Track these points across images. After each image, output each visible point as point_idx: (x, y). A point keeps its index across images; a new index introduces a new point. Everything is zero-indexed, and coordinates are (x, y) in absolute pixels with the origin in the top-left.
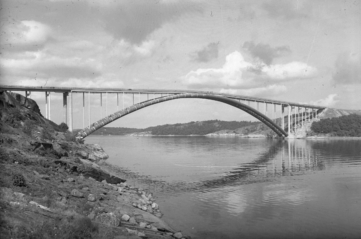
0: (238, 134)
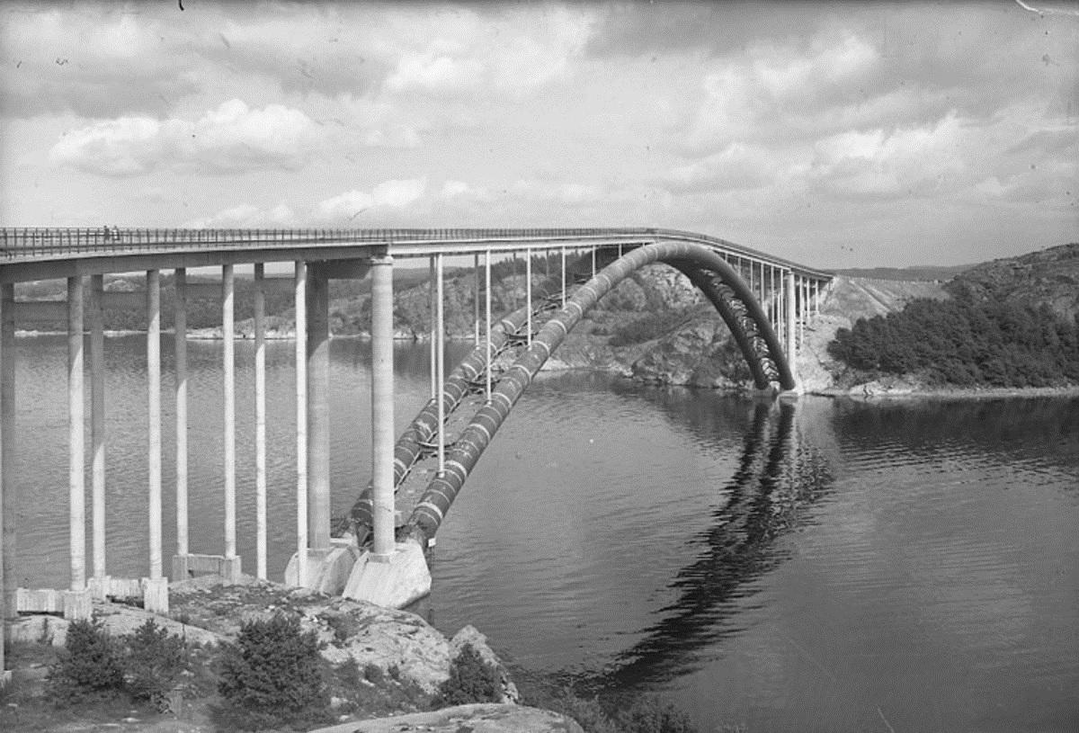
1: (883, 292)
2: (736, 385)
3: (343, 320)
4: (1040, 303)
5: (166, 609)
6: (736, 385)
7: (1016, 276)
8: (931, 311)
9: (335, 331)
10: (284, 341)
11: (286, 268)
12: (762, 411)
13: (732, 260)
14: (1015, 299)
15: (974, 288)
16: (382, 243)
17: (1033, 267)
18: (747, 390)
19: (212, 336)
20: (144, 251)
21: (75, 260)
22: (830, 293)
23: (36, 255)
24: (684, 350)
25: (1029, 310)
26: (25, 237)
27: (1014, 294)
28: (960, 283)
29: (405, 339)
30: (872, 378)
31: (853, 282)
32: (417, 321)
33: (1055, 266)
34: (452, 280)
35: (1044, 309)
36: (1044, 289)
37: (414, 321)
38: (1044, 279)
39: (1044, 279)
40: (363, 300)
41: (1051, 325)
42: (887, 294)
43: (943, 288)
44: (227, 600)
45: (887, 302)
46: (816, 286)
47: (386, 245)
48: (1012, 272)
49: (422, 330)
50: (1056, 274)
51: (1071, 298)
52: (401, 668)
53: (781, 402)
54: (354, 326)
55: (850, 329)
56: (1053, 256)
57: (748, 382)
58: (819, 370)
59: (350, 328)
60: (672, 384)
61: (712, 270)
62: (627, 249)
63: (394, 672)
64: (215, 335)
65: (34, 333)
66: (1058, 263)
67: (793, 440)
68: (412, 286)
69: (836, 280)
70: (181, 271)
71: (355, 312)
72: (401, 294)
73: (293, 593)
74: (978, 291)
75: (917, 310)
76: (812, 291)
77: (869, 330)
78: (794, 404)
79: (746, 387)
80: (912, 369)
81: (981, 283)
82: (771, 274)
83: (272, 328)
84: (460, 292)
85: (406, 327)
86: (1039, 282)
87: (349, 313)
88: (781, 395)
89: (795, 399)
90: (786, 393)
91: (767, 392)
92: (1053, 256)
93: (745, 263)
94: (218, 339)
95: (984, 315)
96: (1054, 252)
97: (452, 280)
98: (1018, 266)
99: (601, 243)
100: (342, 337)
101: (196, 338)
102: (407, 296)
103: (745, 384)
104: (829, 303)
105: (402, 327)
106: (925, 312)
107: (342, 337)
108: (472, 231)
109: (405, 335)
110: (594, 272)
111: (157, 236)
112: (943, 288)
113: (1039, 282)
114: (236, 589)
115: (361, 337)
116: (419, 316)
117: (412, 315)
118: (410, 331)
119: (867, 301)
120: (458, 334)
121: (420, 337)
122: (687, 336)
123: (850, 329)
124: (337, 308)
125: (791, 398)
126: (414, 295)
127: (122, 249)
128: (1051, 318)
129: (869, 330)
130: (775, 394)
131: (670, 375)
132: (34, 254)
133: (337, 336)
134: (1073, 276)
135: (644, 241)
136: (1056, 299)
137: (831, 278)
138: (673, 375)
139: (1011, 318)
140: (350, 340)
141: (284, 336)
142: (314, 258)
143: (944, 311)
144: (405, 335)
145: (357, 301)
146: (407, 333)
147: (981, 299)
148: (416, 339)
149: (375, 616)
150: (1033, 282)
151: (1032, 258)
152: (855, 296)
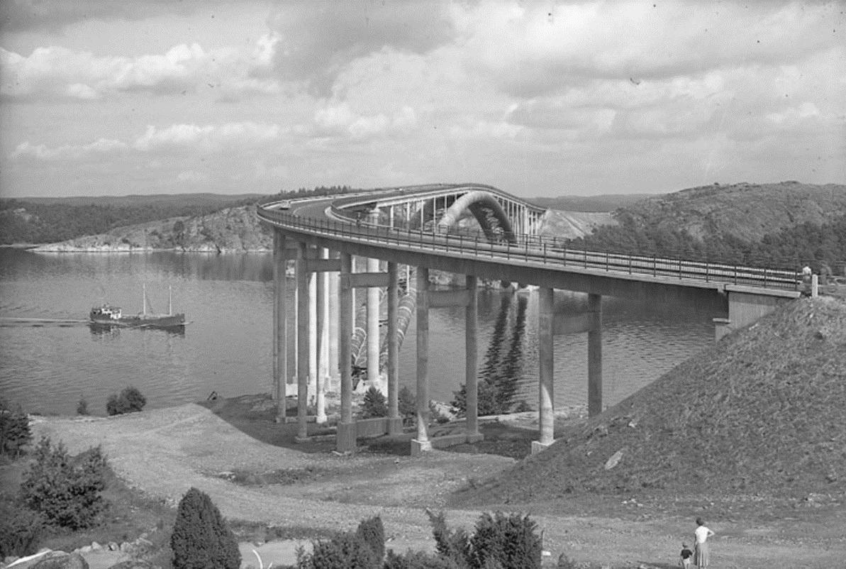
0: (138, 246)
1: (577, 220)
2: (484, 285)
3: (160, 238)
4: (680, 229)
6: (484, 285)
7: (663, 209)
9: (155, 246)
10: (115, 253)
12: (506, 303)
13: (500, 201)
14: (663, 225)
15: (635, 218)
17: (674, 204)
18: (493, 289)
19: (56, 250)
22: (544, 221)
23: (449, 252)
25: (674, 233)
27: (663, 222)
29: (211, 252)
31: (558, 213)
32: (219, 239)
33: (688, 203)
34: (244, 207)
35: (684, 233)
36: (682, 218)
37: (217, 238)
38: (682, 213)
39: (682, 213)
40: (174, 223)
41: (690, 244)
42: (579, 222)
43: (614, 218)
45: (581, 228)
46: (536, 216)
48: (660, 207)
49: (225, 245)
50: (690, 209)
51: (699, 226)
53: (518, 297)
54: (168, 242)
56: (686, 196)
57: (494, 283)
59: (166, 243)
60: (438, 284)
64: (59, 249)
66: (690, 201)
67: (527, 322)
68: (213, 212)
69: (548, 212)
71: (168, 231)
72: (206, 217)
74: (638, 220)
76: (534, 219)
78: (527, 297)
79: (492, 286)
81: (640, 215)
82: (515, 209)
83: (105, 243)
84: (251, 216)
85: (211, 243)
87: (164, 232)
88: (519, 291)
89: (528, 294)
90: (522, 290)
91: (510, 289)
92: (686, 196)
94: (61, 252)
95: (646, 237)
96: (687, 193)
97: (244, 207)
98: (663, 203)
99: (438, 196)
100: (159, 250)
101: (44, 251)
102: (210, 219)
103: (491, 284)
104: (544, 228)
105: (208, 243)
106: (608, 234)
107: (159, 250)
109: (211, 249)
110: (422, 211)
112: (614, 218)
113: (679, 214)
115: (175, 250)
116: (221, 235)
117: (215, 234)
118: (214, 246)
119: (569, 227)
120: (252, 248)
121: (223, 251)
124: (154, 228)
125: (525, 293)
126: (215, 218)
128: (690, 238)
130: (514, 291)
131: (437, 278)
132: (447, 251)
133: (155, 250)
134: (700, 211)
135: (464, 192)
136: (690, 225)
137: (545, 211)
138: (439, 278)
139: (664, 239)
140: (166, 253)
141: (115, 250)
143: (620, 234)
144: (211, 249)
145: (170, 223)
146: (213, 248)
147: (641, 226)
148: (220, 252)
150: (674, 214)
151: (671, 197)
152: (561, 224)
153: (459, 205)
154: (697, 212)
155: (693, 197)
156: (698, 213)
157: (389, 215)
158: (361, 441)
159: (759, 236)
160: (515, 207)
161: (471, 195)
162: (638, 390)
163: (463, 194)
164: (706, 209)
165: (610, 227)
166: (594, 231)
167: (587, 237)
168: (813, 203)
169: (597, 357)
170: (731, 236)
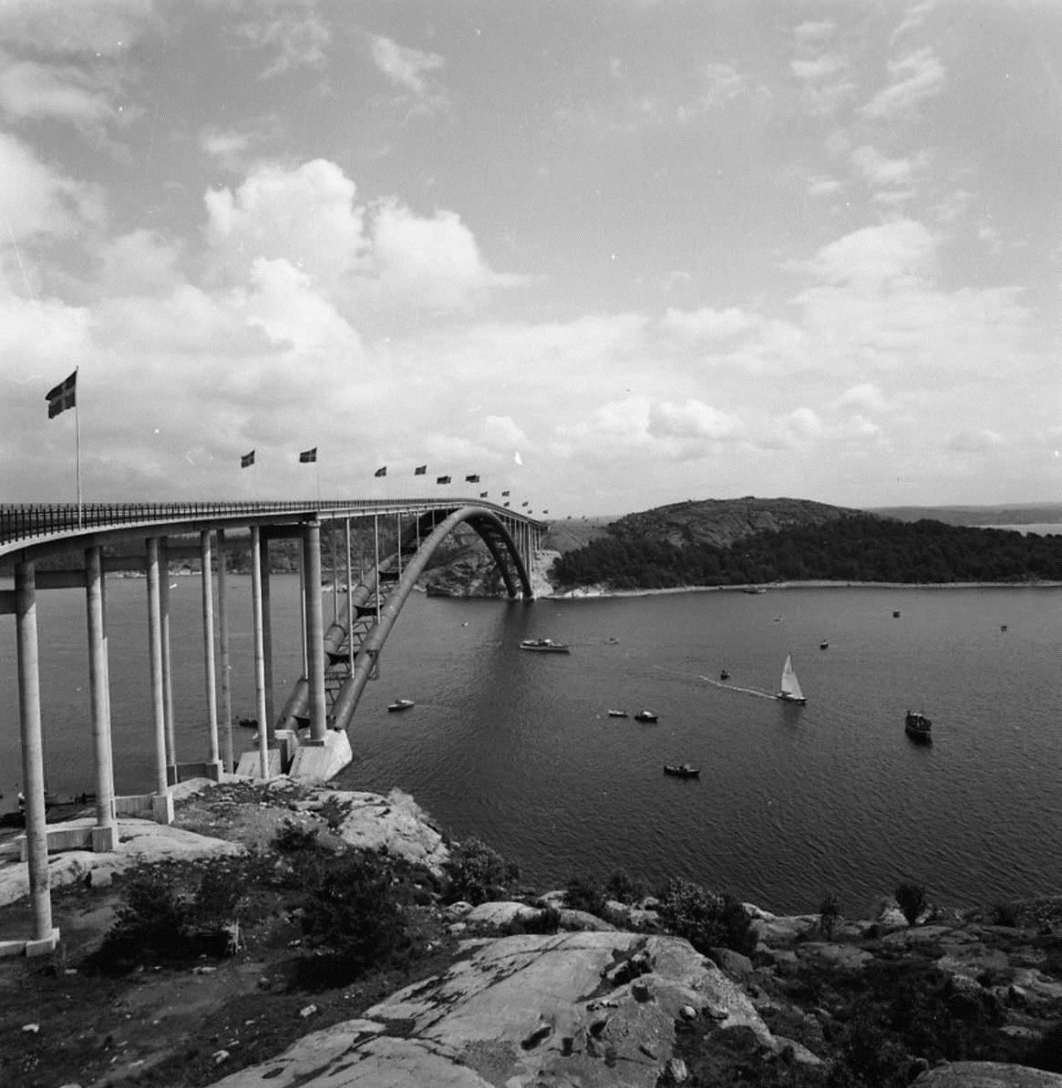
5: (752, 971)
8: (606, 545)
11: (244, 531)
13: (502, 517)
14: (649, 535)
16: (311, 511)
20: (239, 515)
21: (92, 534)
24: (460, 575)
25: (658, 543)
26: (92, 510)
28: (615, 528)
30: (576, 587)
35: (666, 542)
41: (672, 552)
44: (221, 801)
46: (540, 532)
47: (316, 513)
52: (388, 845)
55: (561, 558)
58: (546, 584)
61: (490, 524)
62: (454, 510)
63: (384, 850)
65: (694, 588)
70: (221, 533)
73: (271, 786)
75: (595, 546)
76: (537, 535)
77: (572, 558)
80: (599, 582)
86: (661, 526)
93: (508, 520)
108: (330, 502)
111: (196, 508)
113: (661, 526)
114: (225, 789)
122: (461, 566)
123: (561, 558)
127: (137, 521)
129: (572, 558)
142: (266, 523)
149: (350, 802)
153: (456, 516)
154: (674, 524)
155: (671, 512)
156: (677, 525)
157: (396, 534)
158: (566, 653)
159: (728, 542)
160: (522, 525)
161: (467, 510)
162: (482, 1080)
163: (457, 509)
164: (683, 521)
165: (603, 539)
166: (591, 543)
167: (584, 549)
168: (769, 513)
169: (359, 787)
170: (706, 543)
